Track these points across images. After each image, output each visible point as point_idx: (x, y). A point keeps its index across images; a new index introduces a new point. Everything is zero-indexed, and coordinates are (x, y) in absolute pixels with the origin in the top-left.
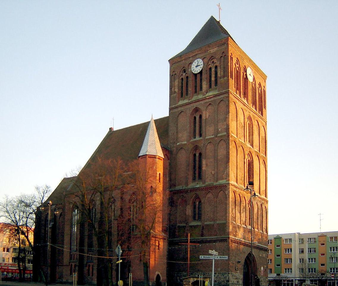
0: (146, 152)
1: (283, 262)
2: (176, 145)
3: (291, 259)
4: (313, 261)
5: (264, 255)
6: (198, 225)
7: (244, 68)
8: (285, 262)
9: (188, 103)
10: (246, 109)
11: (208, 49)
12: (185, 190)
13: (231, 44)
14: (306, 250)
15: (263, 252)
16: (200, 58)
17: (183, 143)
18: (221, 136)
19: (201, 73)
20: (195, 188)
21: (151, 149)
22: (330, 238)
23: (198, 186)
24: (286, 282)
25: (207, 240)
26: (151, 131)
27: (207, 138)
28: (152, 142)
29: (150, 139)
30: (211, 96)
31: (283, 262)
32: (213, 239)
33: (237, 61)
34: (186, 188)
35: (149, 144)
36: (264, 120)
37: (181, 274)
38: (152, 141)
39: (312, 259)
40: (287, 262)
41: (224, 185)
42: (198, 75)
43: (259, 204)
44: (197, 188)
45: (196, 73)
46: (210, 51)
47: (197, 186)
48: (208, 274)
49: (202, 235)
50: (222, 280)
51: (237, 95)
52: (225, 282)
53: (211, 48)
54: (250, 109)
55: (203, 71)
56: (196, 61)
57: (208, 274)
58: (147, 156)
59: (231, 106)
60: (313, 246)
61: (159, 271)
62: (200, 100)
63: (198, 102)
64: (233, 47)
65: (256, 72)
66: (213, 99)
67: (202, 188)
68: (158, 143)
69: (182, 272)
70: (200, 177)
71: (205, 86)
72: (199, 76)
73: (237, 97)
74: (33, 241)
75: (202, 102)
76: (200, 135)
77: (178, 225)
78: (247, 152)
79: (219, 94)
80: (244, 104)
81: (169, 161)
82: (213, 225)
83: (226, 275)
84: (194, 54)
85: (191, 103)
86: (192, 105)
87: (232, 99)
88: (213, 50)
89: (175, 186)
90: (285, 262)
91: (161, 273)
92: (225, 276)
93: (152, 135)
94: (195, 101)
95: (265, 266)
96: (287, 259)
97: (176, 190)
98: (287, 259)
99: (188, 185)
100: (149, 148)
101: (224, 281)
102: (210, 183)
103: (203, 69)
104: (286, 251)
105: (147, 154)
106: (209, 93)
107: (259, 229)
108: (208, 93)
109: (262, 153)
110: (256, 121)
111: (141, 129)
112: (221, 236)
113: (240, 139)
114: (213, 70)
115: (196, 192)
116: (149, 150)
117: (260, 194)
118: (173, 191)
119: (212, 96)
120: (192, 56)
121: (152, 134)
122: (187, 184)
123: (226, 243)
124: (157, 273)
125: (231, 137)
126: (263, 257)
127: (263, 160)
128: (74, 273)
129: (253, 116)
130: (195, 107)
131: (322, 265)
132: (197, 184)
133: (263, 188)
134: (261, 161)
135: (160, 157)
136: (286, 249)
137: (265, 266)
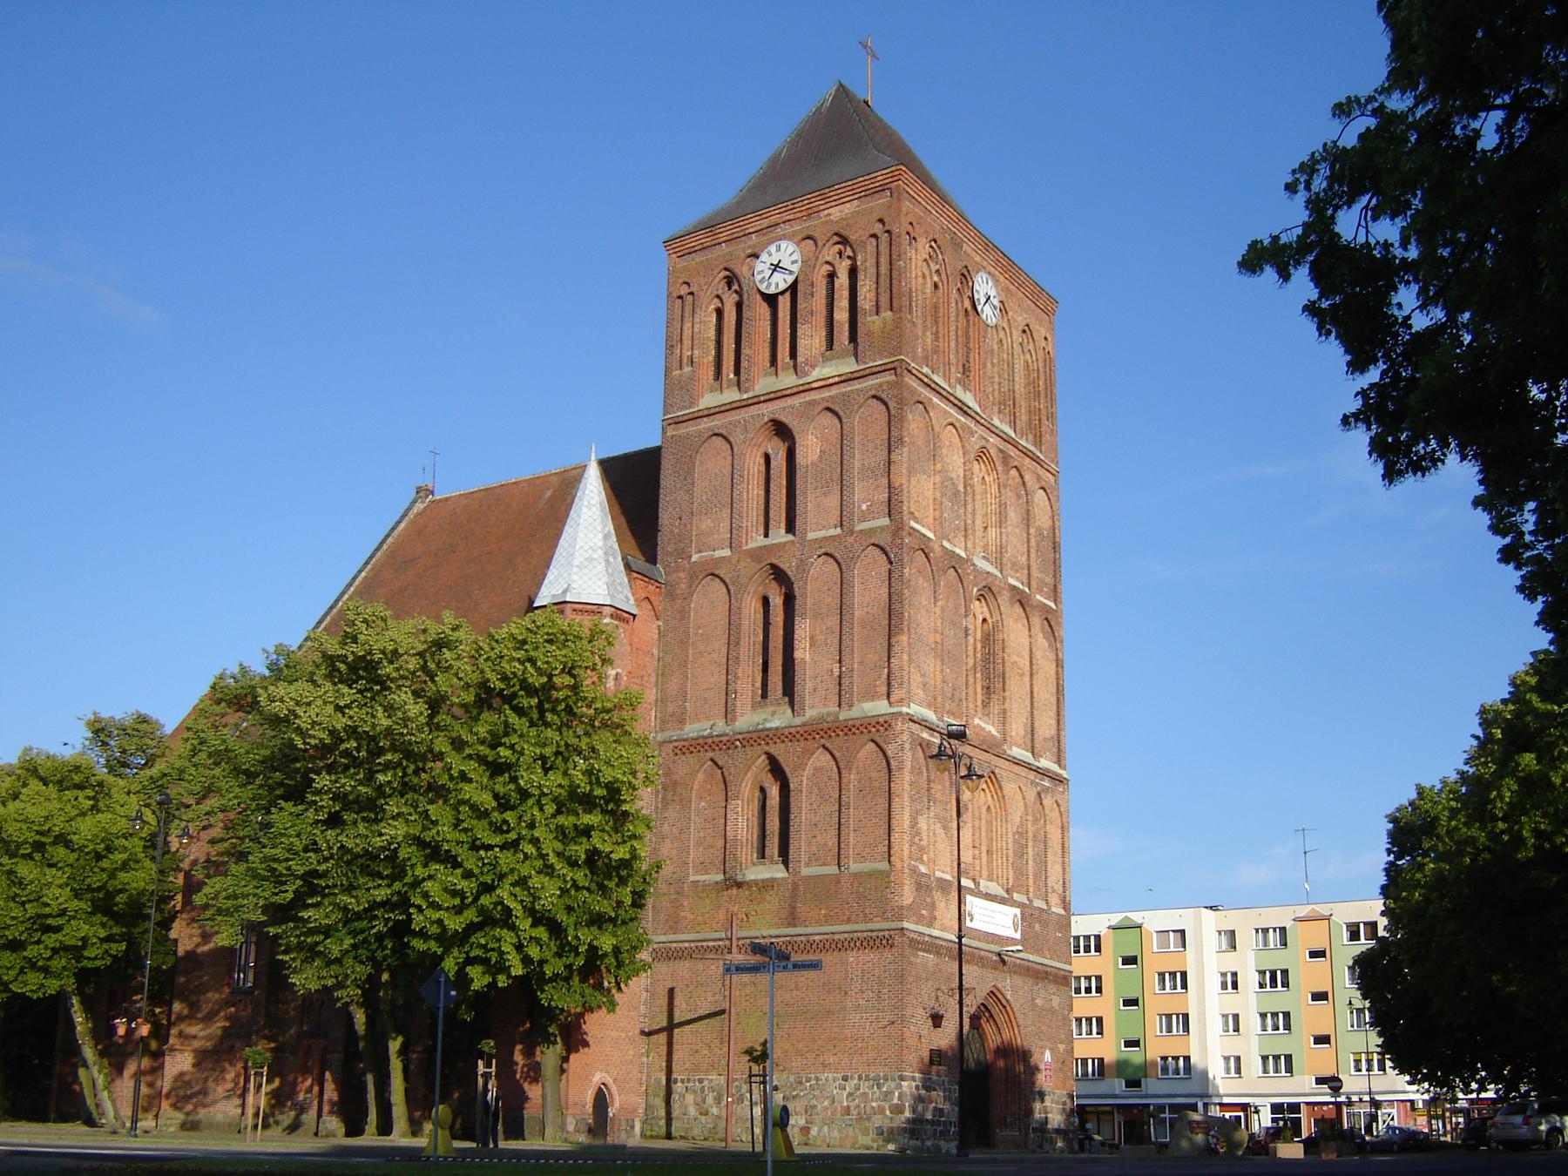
0: (565, 592)
1: (1155, 1026)
2: (689, 563)
3: (1186, 1016)
4: (1091, 1031)
5: (1056, 1001)
6: (774, 880)
7: (962, 274)
8: (1161, 1032)
9: (739, 404)
10: (972, 426)
11: (821, 207)
12: (724, 739)
13: (909, 190)
14: (1249, 980)
15: (1052, 988)
16: (790, 239)
17: (718, 554)
18: (872, 531)
19: (793, 288)
20: (762, 730)
21: (586, 579)
22: (1349, 926)
23: (775, 723)
24: (1167, 1115)
25: (811, 938)
26: (585, 510)
27: (811, 536)
28: (590, 551)
29: (580, 543)
30: (831, 381)
31: (1155, 1026)
32: (836, 937)
33: (935, 251)
34: (728, 730)
35: (576, 562)
36: (1046, 466)
37: (701, 1081)
38: (591, 548)
39: (1089, 1020)
40: (1169, 1030)
41: (881, 720)
42: (780, 297)
43: (1031, 795)
44: (770, 729)
45: (772, 290)
46: (826, 212)
47: (768, 725)
48: (813, 1082)
49: (792, 919)
50: (874, 1104)
51: (935, 378)
52: (888, 1112)
53: (834, 203)
54: (989, 426)
55: (800, 287)
56: (773, 248)
57: (813, 1082)
58: (569, 605)
59: (910, 417)
60: (1277, 960)
61: (607, 1072)
62: (789, 392)
63: (778, 401)
64: (919, 199)
65: (1012, 287)
66: (838, 391)
67: (793, 730)
68: (615, 558)
69: (707, 1072)
70: (789, 690)
71: (811, 339)
72: (784, 304)
73: (933, 385)
74: (847, 305)
75: (796, 401)
76: (790, 528)
77: (692, 878)
78: (975, 590)
79: (861, 373)
80: (965, 409)
81: (661, 623)
82: (836, 880)
83: (889, 1083)
84: (765, 223)
85: (750, 401)
86: (754, 410)
87: (913, 392)
88: (841, 211)
89: (682, 722)
90: (1161, 1032)
91: (615, 1080)
92: (884, 1089)
93: (590, 524)
94: (767, 397)
95: (1061, 1047)
96: (1169, 1016)
97: (685, 740)
98: (1169, 1016)
99: (734, 719)
100: (575, 577)
101: (881, 1111)
102: (825, 711)
103: (800, 279)
104: (1163, 980)
105: (568, 600)
106: (823, 367)
107: (1031, 895)
108: (817, 369)
109: (1041, 592)
110: (1014, 472)
111: (549, 494)
112: (870, 926)
113: (949, 540)
114: (843, 280)
115: (767, 748)
116: (574, 586)
117: (1033, 753)
118: (675, 741)
119: (837, 379)
120: (758, 228)
121: (590, 520)
122: (729, 714)
123: (888, 955)
124: (597, 1078)
125: (910, 534)
126: (1052, 1011)
127: (1047, 619)
128: (370, 1078)
129: (1001, 451)
130: (766, 419)
131: (1129, 1044)
132: (774, 713)
133: (1046, 728)
134: (1037, 621)
135: (619, 612)
136: (1162, 975)
137: (1061, 1047)
